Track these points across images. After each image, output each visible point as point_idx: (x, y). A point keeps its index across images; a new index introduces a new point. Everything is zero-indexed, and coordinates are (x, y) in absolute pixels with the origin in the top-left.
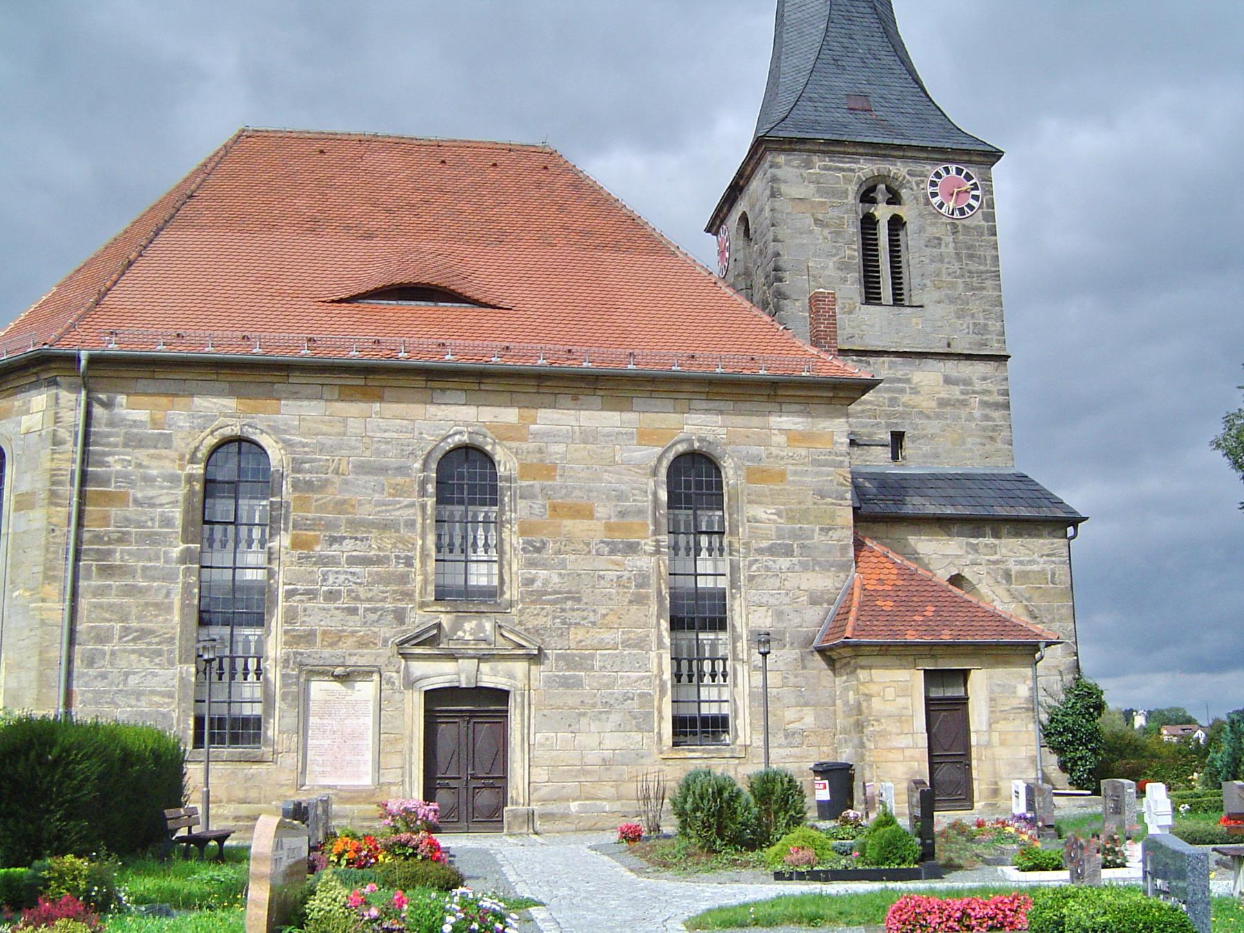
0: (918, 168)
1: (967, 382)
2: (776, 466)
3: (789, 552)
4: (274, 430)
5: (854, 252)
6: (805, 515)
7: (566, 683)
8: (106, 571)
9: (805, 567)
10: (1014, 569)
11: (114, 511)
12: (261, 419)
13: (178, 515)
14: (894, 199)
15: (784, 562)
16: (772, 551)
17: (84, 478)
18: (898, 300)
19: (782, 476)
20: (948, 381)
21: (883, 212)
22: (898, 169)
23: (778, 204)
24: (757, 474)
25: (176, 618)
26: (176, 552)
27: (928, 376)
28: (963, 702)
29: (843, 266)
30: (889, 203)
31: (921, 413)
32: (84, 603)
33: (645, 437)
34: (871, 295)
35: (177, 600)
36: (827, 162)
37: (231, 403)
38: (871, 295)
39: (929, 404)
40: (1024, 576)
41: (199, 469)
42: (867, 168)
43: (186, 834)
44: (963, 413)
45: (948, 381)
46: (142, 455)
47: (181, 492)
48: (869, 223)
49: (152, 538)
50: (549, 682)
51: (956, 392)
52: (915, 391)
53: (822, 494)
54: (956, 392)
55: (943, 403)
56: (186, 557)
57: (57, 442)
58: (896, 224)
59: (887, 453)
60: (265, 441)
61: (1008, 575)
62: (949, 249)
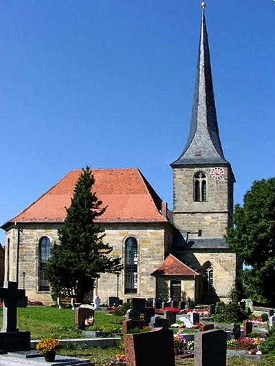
0: (208, 169)
1: (218, 218)
2: (148, 240)
3: (150, 257)
4: (51, 235)
5: (192, 190)
6: (154, 250)
7: (104, 282)
8: (23, 261)
9: (153, 260)
10: (222, 260)
11: (24, 250)
12: (48, 233)
13: (35, 251)
14: (204, 176)
15: (149, 259)
16: (146, 257)
17: (19, 244)
18: (203, 200)
19: (149, 242)
20: (213, 218)
21: (200, 180)
22: (204, 169)
23: (175, 180)
24: (144, 242)
25: (35, 268)
26: (35, 257)
27: (208, 217)
28: (180, 287)
29: (189, 193)
30: (202, 177)
31: (206, 226)
32: (19, 266)
33: (121, 235)
34: (197, 199)
35: (35, 266)
36: (187, 169)
37: (43, 230)
38: (197, 199)
39: (208, 224)
40: (224, 261)
41: (38, 242)
42: (196, 170)
43: (192, 283)
44: (216, 225)
45: (213, 218)
46: (28, 240)
47: (35, 247)
48: (197, 183)
49: (32, 255)
50: (101, 281)
51: (214, 220)
52: (205, 221)
53: (158, 245)
54: (214, 220)
55: (211, 223)
56: (36, 258)
57: (14, 238)
58: (204, 182)
59: (197, 235)
60: (49, 237)
61: (220, 261)
62: (215, 187)
